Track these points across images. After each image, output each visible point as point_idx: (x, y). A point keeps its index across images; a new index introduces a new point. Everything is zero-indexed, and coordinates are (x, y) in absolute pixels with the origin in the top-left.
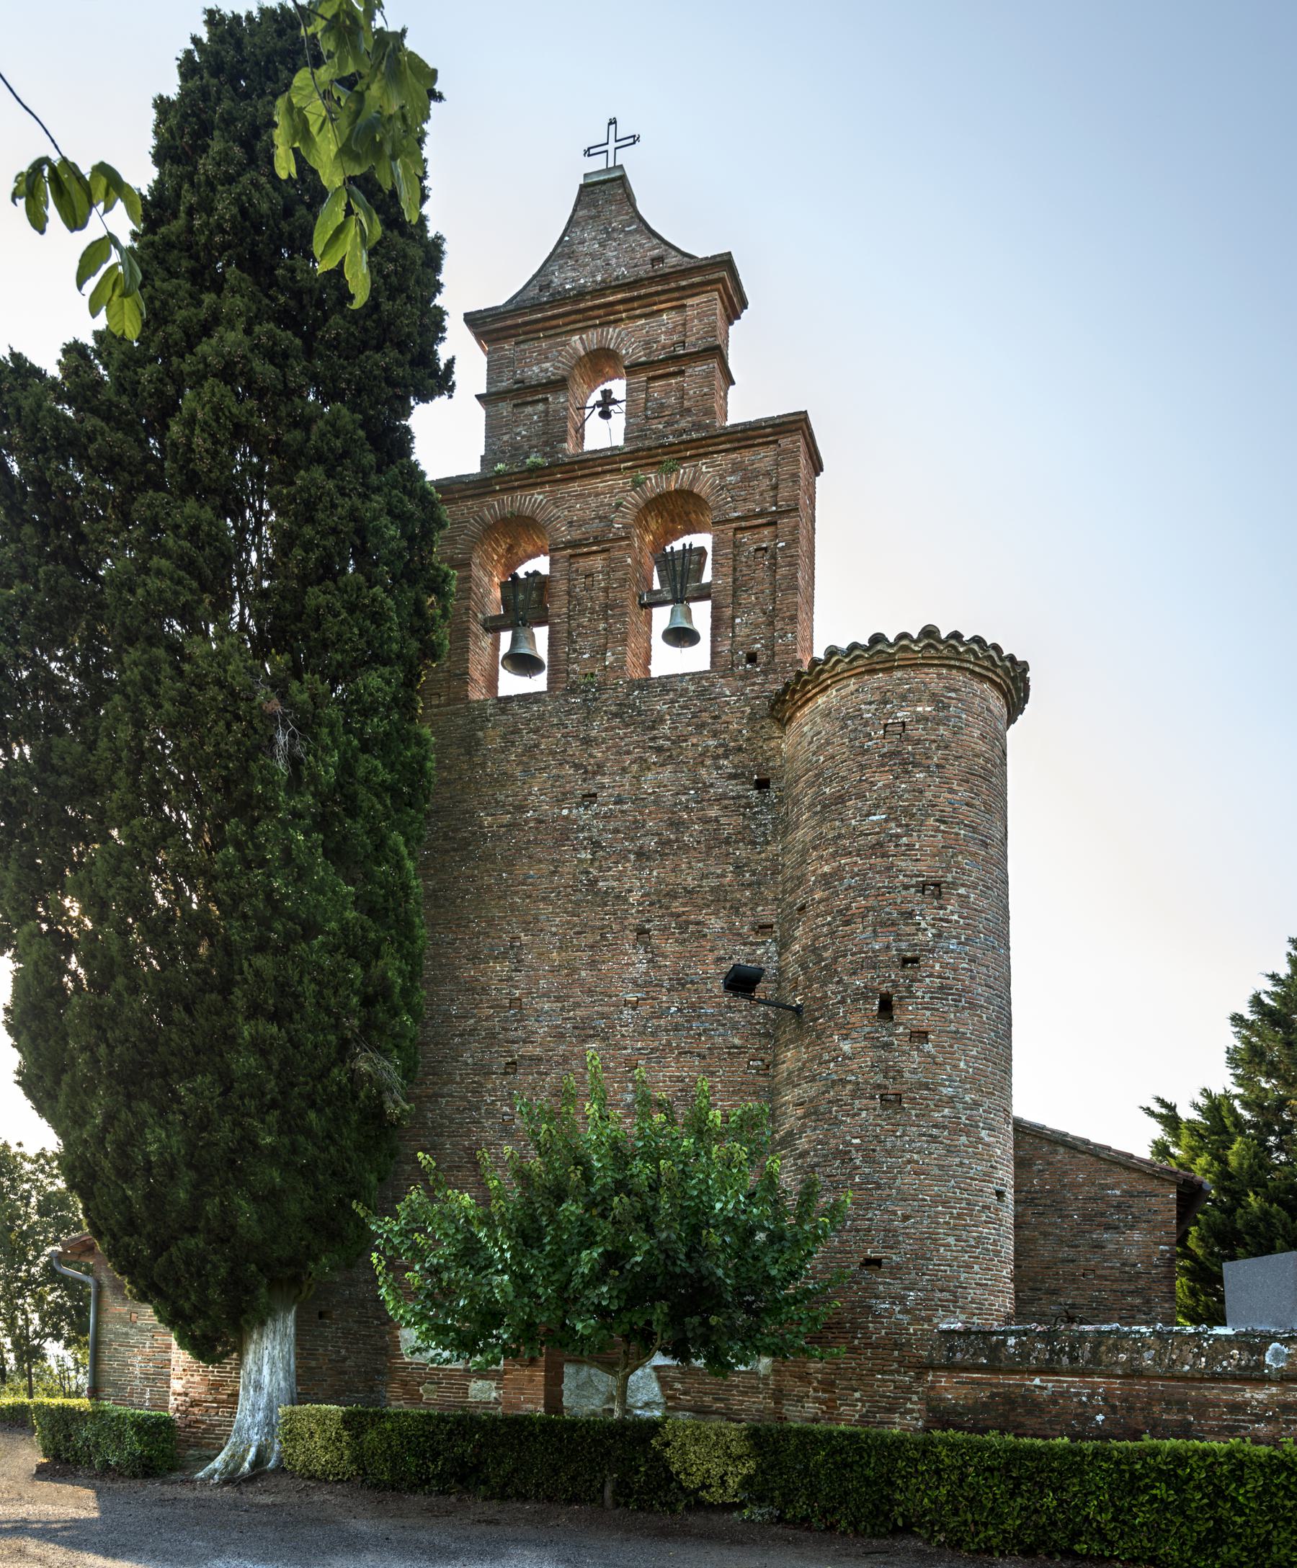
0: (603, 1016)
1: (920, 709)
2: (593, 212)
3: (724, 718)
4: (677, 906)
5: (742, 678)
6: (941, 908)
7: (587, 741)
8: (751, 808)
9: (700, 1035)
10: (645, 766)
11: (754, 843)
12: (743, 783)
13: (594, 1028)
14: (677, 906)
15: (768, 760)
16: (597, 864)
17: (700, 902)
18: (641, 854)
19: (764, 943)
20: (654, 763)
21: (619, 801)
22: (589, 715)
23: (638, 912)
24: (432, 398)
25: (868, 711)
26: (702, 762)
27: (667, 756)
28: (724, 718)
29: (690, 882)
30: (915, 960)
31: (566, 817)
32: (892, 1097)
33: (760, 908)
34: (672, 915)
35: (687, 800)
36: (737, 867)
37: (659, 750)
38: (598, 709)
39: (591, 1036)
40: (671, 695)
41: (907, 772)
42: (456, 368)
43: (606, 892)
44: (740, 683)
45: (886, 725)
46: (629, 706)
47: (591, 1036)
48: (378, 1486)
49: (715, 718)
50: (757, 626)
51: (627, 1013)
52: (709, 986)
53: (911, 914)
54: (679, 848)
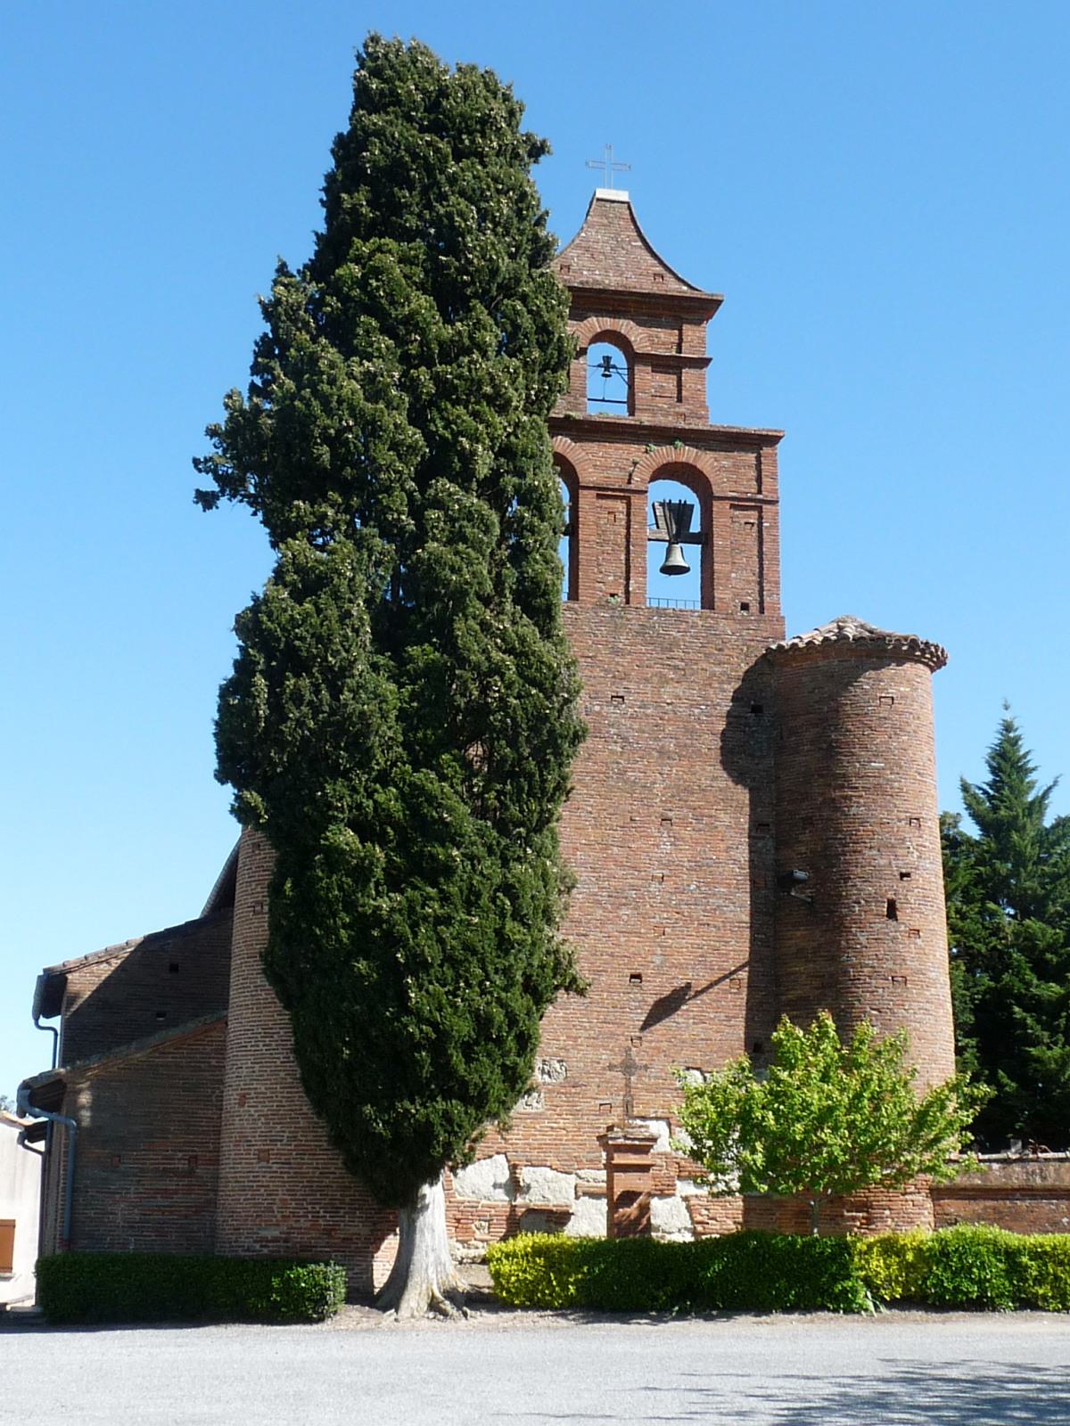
0: (633, 888)
1: (902, 689)
2: (605, 221)
3: (726, 652)
4: (694, 800)
5: (740, 622)
6: (921, 837)
7: (616, 652)
8: (750, 727)
9: (715, 910)
10: (664, 681)
11: (752, 756)
12: (743, 707)
13: (626, 898)
14: (694, 800)
15: (762, 691)
16: (626, 756)
17: (712, 799)
18: (662, 752)
19: (763, 838)
20: (672, 679)
21: (644, 706)
22: (616, 629)
23: (661, 801)
24: (327, 223)
25: (868, 684)
26: (710, 685)
27: (683, 675)
28: (726, 652)
29: (705, 782)
30: (908, 875)
31: (599, 713)
32: (900, 979)
33: (759, 809)
34: (689, 807)
35: (700, 714)
36: (741, 774)
37: (676, 668)
38: (623, 625)
39: (624, 905)
40: (684, 626)
41: (896, 734)
42: (1032, 745)
43: (634, 782)
44: (738, 626)
45: (881, 697)
46: (650, 628)
47: (624, 905)
48: (893, 1304)
49: (720, 650)
50: (749, 582)
51: (654, 887)
52: (721, 869)
53: (904, 840)
54: (693, 751)
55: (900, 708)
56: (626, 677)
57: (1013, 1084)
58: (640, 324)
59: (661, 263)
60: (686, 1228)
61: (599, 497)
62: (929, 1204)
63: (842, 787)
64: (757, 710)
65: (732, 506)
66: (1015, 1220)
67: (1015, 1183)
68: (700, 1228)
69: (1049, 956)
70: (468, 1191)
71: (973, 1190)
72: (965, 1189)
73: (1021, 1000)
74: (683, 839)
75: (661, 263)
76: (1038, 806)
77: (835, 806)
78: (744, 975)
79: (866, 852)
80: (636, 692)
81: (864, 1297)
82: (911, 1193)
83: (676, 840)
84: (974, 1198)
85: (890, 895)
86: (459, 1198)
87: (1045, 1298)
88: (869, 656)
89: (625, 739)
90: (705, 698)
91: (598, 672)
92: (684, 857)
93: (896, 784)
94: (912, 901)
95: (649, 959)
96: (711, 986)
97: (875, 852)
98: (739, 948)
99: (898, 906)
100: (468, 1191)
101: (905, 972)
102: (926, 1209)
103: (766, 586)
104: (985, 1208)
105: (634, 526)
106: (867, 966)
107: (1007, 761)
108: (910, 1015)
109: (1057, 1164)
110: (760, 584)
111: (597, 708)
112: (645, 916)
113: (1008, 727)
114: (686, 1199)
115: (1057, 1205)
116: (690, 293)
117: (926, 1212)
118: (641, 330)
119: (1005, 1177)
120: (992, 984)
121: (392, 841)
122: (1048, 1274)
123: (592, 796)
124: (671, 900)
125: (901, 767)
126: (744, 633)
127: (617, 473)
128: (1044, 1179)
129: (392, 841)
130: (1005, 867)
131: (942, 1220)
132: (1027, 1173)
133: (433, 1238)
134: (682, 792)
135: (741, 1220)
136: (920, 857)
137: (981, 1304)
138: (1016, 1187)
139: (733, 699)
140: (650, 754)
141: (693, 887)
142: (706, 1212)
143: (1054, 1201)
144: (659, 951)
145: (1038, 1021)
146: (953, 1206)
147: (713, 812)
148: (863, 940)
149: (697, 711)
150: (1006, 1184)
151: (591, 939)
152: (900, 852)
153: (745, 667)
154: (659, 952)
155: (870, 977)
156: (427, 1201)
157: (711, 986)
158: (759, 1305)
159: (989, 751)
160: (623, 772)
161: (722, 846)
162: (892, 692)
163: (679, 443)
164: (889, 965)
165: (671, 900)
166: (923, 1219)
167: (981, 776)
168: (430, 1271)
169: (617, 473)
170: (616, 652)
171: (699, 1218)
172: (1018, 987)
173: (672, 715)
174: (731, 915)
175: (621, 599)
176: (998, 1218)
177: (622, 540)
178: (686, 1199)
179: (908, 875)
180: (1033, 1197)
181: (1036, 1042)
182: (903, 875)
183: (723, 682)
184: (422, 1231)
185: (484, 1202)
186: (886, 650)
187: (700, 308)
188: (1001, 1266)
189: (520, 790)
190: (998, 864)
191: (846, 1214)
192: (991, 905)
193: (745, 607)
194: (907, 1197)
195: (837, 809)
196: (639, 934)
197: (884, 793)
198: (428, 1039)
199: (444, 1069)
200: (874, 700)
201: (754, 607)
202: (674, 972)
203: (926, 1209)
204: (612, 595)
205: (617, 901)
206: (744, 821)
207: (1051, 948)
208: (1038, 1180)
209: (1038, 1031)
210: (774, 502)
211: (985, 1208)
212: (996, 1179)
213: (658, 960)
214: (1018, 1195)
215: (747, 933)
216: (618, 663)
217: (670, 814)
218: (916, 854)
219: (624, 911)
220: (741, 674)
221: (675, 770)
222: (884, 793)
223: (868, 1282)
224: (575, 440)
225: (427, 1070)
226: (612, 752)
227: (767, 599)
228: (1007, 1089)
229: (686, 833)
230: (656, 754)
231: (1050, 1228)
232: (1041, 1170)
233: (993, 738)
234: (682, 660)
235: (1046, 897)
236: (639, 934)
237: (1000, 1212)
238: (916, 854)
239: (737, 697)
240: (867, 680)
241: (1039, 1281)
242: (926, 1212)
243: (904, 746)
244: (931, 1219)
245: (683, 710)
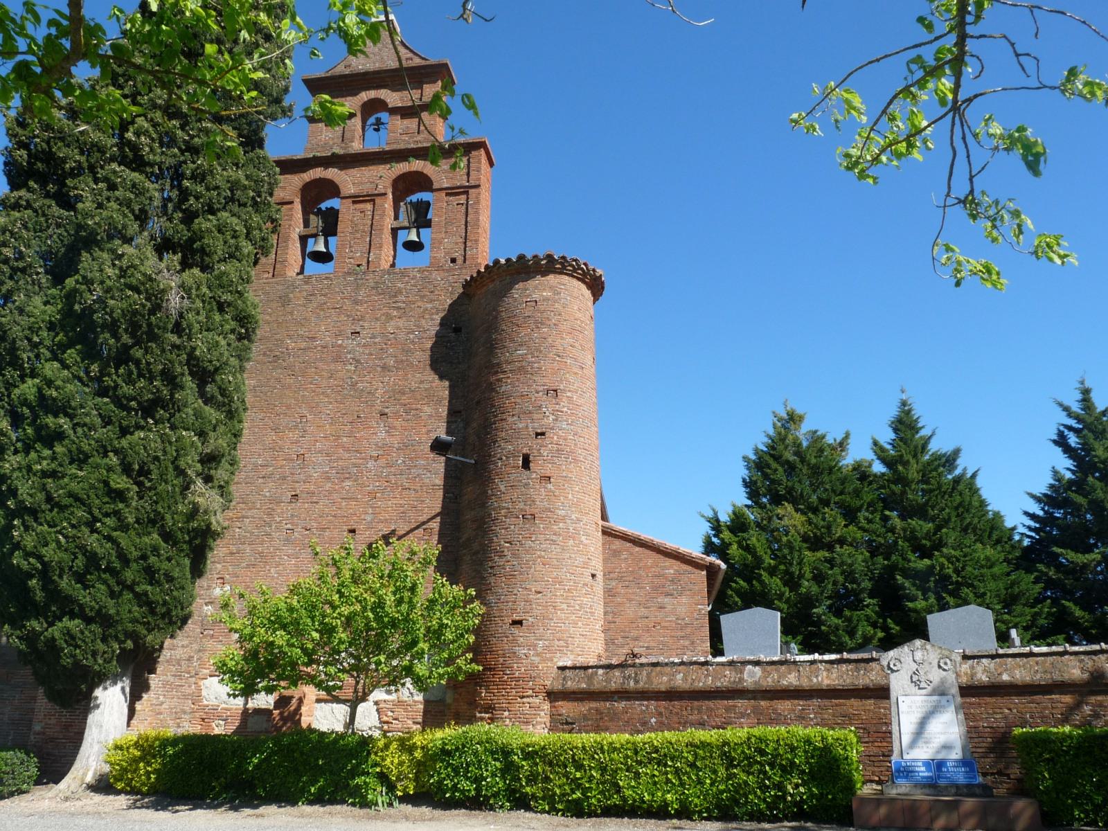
0: (355, 465)
3: (436, 293)
4: (404, 399)
5: (448, 271)
10: (389, 318)
17: (419, 397)
19: (456, 422)
21: (373, 337)
22: (358, 287)
27: (403, 313)
28: (436, 293)
30: (543, 434)
37: (399, 308)
48: (406, 799)
50: (457, 243)
51: (371, 464)
55: (542, 308)
56: (362, 319)
57: (898, 628)
58: (394, 90)
59: (411, 51)
60: (375, 727)
61: (354, 202)
62: (546, 706)
63: (497, 372)
64: (457, 330)
65: (447, 194)
66: (611, 720)
67: (613, 686)
68: (386, 727)
69: (924, 542)
70: (212, 697)
71: (581, 693)
72: (574, 693)
73: (906, 573)
74: (394, 428)
75: (411, 51)
76: (924, 447)
77: (491, 388)
78: (435, 525)
79: (510, 419)
80: (367, 328)
81: (378, 793)
82: (528, 697)
83: (390, 430)
84: (582, 700)
85: (525, 451)
86: (205, 703)
87: (534, 796)
88: (519, 273)
89: (358, 361)
90: (418, 326)
91: (343, 318)
92: (395, 441)
93: (536, 365)
94: (545, 454)
95: (363, 517)
96: (408, 533)
97: (515, 418)
98: (434, 503)
99: (531, 458)
100: (212, 697)
101: (534, 511)
102: (543, 710)
103: (469, 244)
104: (590, 709)
105: (376, 217)
106: (504, 508)
107: (905, 424)
108: (536, 545)
109: (650, 669)
110: (465, 243)
111: (340, 342)
112: (363, 485)
113: (904, 403)
114: (376, 703)
115: (647, 706)
116: (423, 63)
117: (542, 714)
118: (394, 94)
119: (606, 681)
120: (886, 562)
121: (28, 418)
122: (538, 774)
123: (331, 403)
124: (382, 472)
125: (541, 352)
126: (450, 278)
127: (368, 185)
128: (637, 682)
129: (28, 418)
130: (897, 488)
131: (560, 724)
132: (624, 677)
133: (100, 732)
134: (396, 394)
135: (421, 720)
136: (557, 420)
137: (477, 803)
138: (613, 689)
139: (441, 324)
140: (375, 370)
141: (400, 462)
142: (391, 714)
143: (645, 703)
144: (370, 511)
145: (914, 585)
146: (567, 709)
147: (419, 406)
148: (502, 488)
149: (412, 336)
150: (605, 687)
151: (320, 506)
152: (535, 416)
153: (449, 302)
154: (370, 511)
155: (506, 517)
156: (98, 702)
157: (408, 533)
158: (285, 796)
159: (920, 425)
160: (354, 385)
161: (424, 430)
162: (535, 296)
163: (411, 159)
164: (521, 506)
165: (382, 472)
166: (539, 719)
167: (886, 436)
168: (90, 760)
169: (368, 185)
170: (356, 302)
171: (385, 719)
172: (901, 563)
173: (393, 341)
174: (428, 481)
175: (364, 268)
176: (763, 719)
177: (367, 229)
178: (376, 703)
179: (543, 434)
180: (628, 699)
181: (913, 599)
182: (537, 434)
183: (433, 314)
184: (90, 727)
185: (224, 706)
186: (529, 267)
187: (439, 72)
188: (498, 764)
189: (130, 373)
190: (893, 486)
191: (478, 715)
192: (887, 513)
193: (453, 261)
194: (525, 700)
195: (493, 390)
196: (356, 499)
197: (526, 372)
198: (36, 569)
199: (53, 593)
200: (521, 304)
201: (460, 261)
202: (381, 526)
203: (543, 710)
204: (359, 266)
205: (342, 476)
206: (444, 411)
207: (927, 536)
208: (632, 683)
209: (914, 591)
210: (477, 186)
211: (590, 709)
212: (598, 683)
213: (369, 518)
214: (616, 698)
215: (440, 493)
216: (357, 310)
217: (386, 410)
218: (551, 418)
219: (348, 483)
220: (447, 307)
221: (392, 379)
222: (526, 372)
223: (383, 778)
224: (341, 169)
225: (39, 595)
226: (348, 371)
227: (468, 253)
228: (893, 631)
229: (398, 423)
230: (379, 369)
231: (640, 728)
232: (636, 674)
233: (893, 411)
234: (404, 302)
235: (926, 503)
236: (356, 499)
237: (602, 713)
238: (551, 418)
239: (444, 323)
240: (518, 291)
241: (532, 779)
242: (542, 714)
243: (544, 336)
244: (547, 719)
245: (402, 336)
